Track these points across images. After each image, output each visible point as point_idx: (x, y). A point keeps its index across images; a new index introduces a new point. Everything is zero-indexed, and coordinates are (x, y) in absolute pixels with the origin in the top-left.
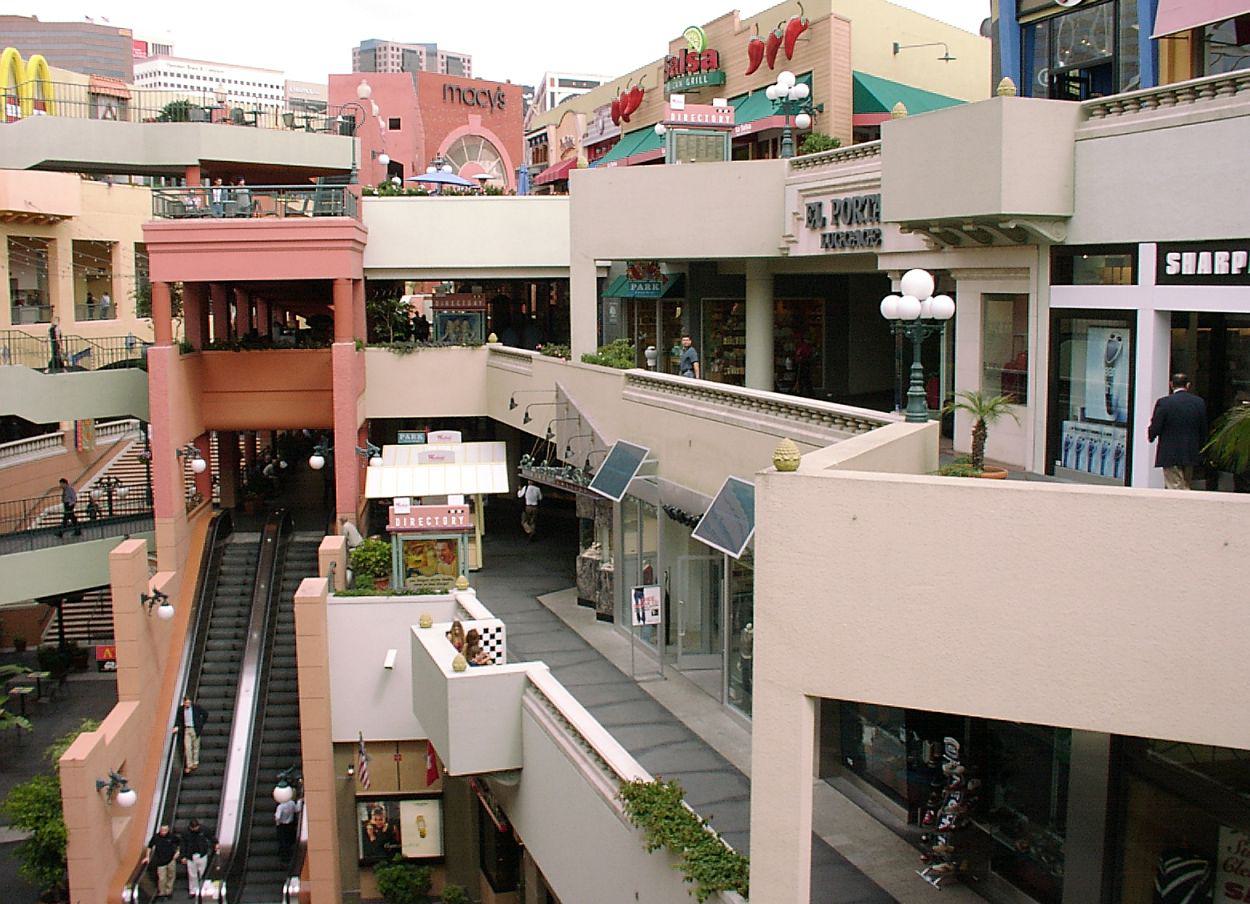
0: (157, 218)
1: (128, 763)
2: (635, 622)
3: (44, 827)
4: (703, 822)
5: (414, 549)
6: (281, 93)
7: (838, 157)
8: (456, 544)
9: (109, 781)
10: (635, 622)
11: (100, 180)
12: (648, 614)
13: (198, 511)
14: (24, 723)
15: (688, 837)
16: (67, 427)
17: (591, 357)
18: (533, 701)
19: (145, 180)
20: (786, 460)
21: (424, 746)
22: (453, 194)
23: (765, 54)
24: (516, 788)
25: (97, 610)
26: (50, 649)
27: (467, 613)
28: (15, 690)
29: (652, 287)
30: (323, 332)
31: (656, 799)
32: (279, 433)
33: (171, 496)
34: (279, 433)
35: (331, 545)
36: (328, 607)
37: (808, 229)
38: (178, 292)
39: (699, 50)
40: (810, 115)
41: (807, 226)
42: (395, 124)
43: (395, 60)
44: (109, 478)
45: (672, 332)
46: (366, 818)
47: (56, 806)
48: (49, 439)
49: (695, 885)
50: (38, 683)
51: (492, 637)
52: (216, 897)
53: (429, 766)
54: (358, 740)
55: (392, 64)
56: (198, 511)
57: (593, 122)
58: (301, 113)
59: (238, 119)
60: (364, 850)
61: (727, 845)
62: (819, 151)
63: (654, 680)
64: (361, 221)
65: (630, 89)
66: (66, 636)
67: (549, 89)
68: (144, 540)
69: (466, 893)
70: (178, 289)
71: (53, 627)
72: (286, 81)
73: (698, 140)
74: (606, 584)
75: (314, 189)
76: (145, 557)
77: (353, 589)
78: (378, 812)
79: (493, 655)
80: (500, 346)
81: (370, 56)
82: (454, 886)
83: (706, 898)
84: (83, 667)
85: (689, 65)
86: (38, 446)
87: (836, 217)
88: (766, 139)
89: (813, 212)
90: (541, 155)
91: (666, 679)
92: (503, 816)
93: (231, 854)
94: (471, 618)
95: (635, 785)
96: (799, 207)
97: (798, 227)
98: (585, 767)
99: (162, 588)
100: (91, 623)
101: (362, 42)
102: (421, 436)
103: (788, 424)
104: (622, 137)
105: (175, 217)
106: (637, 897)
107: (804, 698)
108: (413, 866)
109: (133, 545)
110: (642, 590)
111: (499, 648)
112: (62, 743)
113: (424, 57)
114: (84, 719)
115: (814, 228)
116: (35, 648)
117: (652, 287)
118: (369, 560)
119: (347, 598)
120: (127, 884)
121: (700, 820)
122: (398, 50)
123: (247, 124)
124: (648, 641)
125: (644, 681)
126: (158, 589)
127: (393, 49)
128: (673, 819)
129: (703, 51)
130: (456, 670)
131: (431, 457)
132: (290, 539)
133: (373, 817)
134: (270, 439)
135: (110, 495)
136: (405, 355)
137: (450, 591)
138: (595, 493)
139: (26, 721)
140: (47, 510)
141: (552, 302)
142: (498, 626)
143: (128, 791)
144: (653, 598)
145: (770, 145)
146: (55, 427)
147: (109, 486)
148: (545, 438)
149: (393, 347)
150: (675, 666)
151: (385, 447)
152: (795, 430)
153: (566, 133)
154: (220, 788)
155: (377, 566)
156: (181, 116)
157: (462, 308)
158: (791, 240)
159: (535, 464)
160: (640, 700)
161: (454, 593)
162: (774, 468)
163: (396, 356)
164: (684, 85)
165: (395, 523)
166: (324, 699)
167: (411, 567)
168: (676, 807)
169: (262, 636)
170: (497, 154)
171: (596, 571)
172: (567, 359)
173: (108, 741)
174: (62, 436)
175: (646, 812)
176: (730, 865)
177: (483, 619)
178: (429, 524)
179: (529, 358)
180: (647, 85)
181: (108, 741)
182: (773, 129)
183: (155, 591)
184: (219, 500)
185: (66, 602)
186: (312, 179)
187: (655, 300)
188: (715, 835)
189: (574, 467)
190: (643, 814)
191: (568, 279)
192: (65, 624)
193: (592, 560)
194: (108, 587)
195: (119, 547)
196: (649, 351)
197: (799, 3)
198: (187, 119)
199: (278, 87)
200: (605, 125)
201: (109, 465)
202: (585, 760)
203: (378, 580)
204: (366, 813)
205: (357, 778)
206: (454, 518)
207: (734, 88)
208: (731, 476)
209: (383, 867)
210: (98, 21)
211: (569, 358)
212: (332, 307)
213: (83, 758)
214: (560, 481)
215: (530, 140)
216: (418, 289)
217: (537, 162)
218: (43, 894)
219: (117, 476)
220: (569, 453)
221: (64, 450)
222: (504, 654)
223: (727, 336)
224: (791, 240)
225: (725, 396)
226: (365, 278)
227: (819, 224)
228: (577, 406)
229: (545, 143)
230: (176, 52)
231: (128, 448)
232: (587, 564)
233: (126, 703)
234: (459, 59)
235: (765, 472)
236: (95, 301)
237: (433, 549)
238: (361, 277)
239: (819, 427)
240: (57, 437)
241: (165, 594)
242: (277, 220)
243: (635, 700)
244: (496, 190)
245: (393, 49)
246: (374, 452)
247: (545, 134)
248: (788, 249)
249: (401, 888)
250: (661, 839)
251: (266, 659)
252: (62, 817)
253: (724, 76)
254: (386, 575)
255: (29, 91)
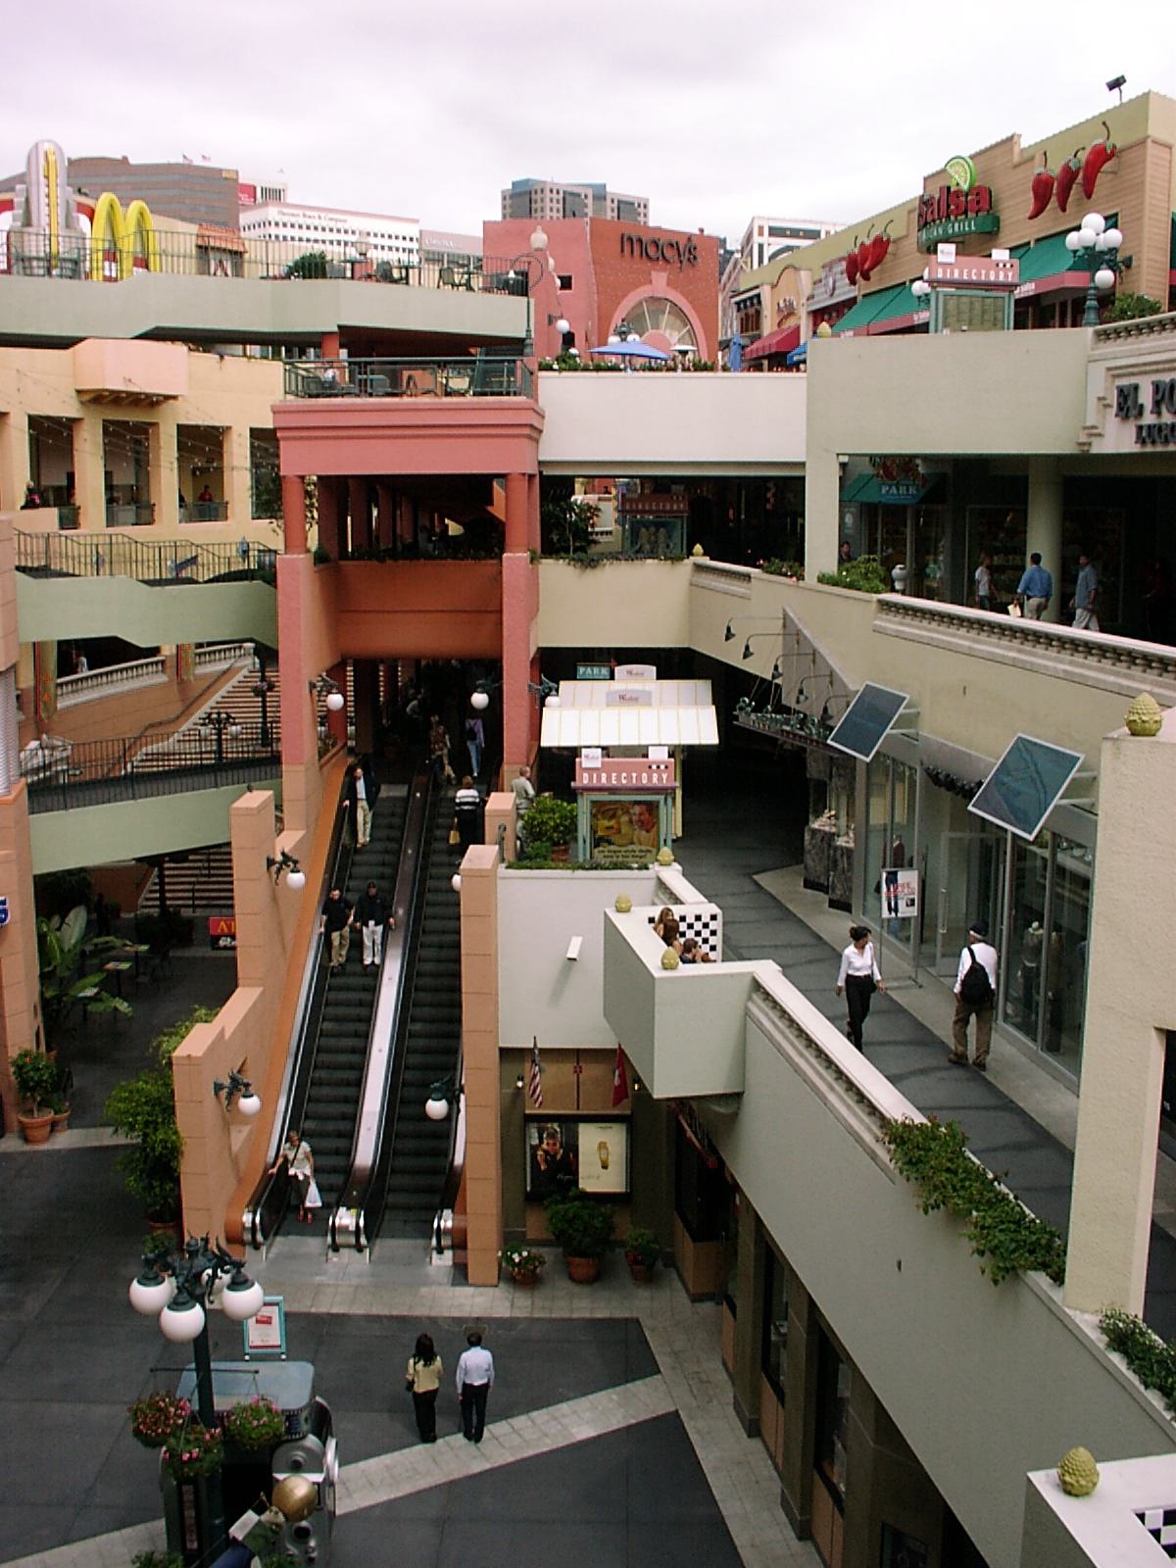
0: (290, 397)
1: (248, 1061)
2: (885, 914)
3: (154, 1134)
4: (995, 1179)
5: (603, 813)
6: (415, 246)
7: (1150, 327)
8: (658, 807)
9: (227, 1082)
10: (885, 914)
11: (209, 352)
12: (902, 904)
13: (331, 758)
14: (123, 1006)
15: (977, 1197)
16: (168, 650)
17: (831, 577)
18: (763, 1011)
19: (262, 351)
20: (1144, 722)
21: (616, 1058)
22: (651, 369)
23: (1054, 191)
24: (733, 1118)
25: (204, 872)
26: (149, 917)
27: (672, 893)
28: (111, 966)
29: (908, 490)
30: (488, 539)
31: (932, 1146)
32: (423, 663)
33: (299, 737)
34: (423, 663)
35: (500, 803)
36: (499, 882)
37: (1118, 419)
38: (309, 488)
39: (965, 187)
40: (1114, 271)
41: (1116, 415)
42: (566, 283)
43: (555, 205)
44: (219, 714)
45: (924, 550)
46: (535, 1142)
47: (169, 1110)
48: (147, 665)
49: (986, 1261)
50: (136, 958)
51: (706, 926)
52: (352, 1228)
53: (617, 1081)
54: (532, 1046)
55: (551, 209)
56: (331, 758)
57: (820, 281)
58: (453, 269)
59: (385, 274)
60: (532, 1183)
61: (1027, 1211)
62: (1133, 317)
63: (906, 987)
64: (537, 401)
65: (872, 238)
66: (168, 902)
67: (756, 239)
68: (271, 792)
69: (656, 1241)
70: (309, 484)
71: (152, 892)
72: (421, 232)
73: (972, 303)
74: (843, 863)
75: (474, 362)
76: (272, 812)
77: (523, 859)
78: (552, 1136)
79: (706, 948)
80: (706, 561)
81: (523, 200)
82: (643, 1230)
83: (1003, 1278)
84: (186, 941)
85: (952, 207)
86: (140, 672)
87: (1157, 404)
88: (1051, 302)
89: (1126, 398)
90: (750, 320)
91: (920, 987)
92: (714, 1150)
93: (370, 1179)
94: (678, 901)
95: (903, 1124)
96: (1106, 389)
97: (1104, 417)
98: (832, 1098)
99: (291, 850)
100: (197, 887)
101: (514, 184)
102: (605, 671)
103: (1102, 670)
104: (860, 299)
105: (310, 396)
106: (899, 1268)
107: (1154, 1033)
108: (592, 1203)
109: (256, 798)
110: (895, 873)
111: (713, 941)
112: (171, 1035)
113: (590, 201)
114: (196, 1006)
115: (1126, 417)
116: (132, 915)
117: (908, 490)
118: (547, 823)
119: (523, 871)
120: (247, 1206)
121: (990, 1176)
122: (558, 192)
123: (395, 281)
124: (896, 937)
125: (892, 989)
126: (286, 851)
127: (551, 191)
128: (955, 1173)
129: (971, 188)
130: (665, 967)
131: (622, 697)
132: (443, 793)
133: (545, 1142)
134: (413, 670)
135: (219, 734)
136: (589, 571)
137: (650, 866)
138: (836, 749)
139: (126, 1004)
140: (144, 750)
141: (768, 506)
142: (714, 913)
143: (252, 1096)
144: (908, 884)
145: (1057, 309)
146: (155, 651)
147: (219, 722)
148: (769, 678)
149: (573, 559)
150: (932, 970)
151: (562, 683)
152: (1112, 679)
153: (785, 294)
154: (357, 1101)
155: (555, 831)
156: (310, 271)
157: (650, 512)
158: (1094, 432)
159: (755, 710)
160: (889, 1012)
161: (655, 869)
162: (1126, 730)
163: (578, 571)
164: (945, 230)
165: (583, 780)
166: (491, 995)
167: (600, 833)
168: (958, 1158)
169: (409, 910)
170: (685, 320)
171: (830, 845)
172: (798, 579)
173: (227, 1035)
174: (163, 662)
175: (919, 1161)
176: (1034, 1238)
177: (693, 904)
178: (624, 782)
179: (747, 577)
180: (894, 233)
181: (227, 1035)
182: (1063, 289)
183: (283, 854)
184: (354, 743)
185: (169, 862)
186: (472, 351)
187: (905, 507)
188: (1011, 1197)
189: (805, 715)
190: (916, 1164)
191: (803, 478)
192: (167, 887)
193: (825, 832)
194: (229, 844)
195: (241, 800)
196: (897, 571)
197: (1104, 123)
198: (324, 276)
199: (411, 239)
200: (837, 284)
201: (217, 697)
202: (832, 1089)
203: (556, 848)
204: (536, 1135)
205: (528, 1092)
206: (655, 776)
207: (1014, 236)
208: (1020, 734)
209: (556, 1203)
210: (198, 162)
211: (801, 577)
212: (490, 509)
213: (200, 1054)
214: (788, 732)
215: (738, 303)
216: (589, 489)
217: (747, 331)
218: (151, 1210)
219: (229, 710)
220: (802, 698)
221: (162, 678)
222: (719, 948)
223: (997, 554)
224: (1094, 432)
225: (981, 625)
226: (541, 473)
227: (1134, 412)
228: (811, 639)
229: (757, 307)
230: (291, 197)
231: (239, 677)
232: (819, 837)
233: (247, 989)
234: (633, 204)
235: (1116, 736)
236: (204, 502)
237: (628, 812)
238: (537, 472)
239: (1144, 675)
240: (157, 663)
241: (295, 858)
242: (436, 400)
243: (884, 1012)
244: (705, 364)
245: (551, 191)
246: (551, 689)
247: (758, 296)
248: (1090, 444)
249: (576, 1230)
250: (941, 1198)
251: (415, 936)
252: (174, 1123)
253: (997, 221)
254: (565, 843)
255: (129, 245)
